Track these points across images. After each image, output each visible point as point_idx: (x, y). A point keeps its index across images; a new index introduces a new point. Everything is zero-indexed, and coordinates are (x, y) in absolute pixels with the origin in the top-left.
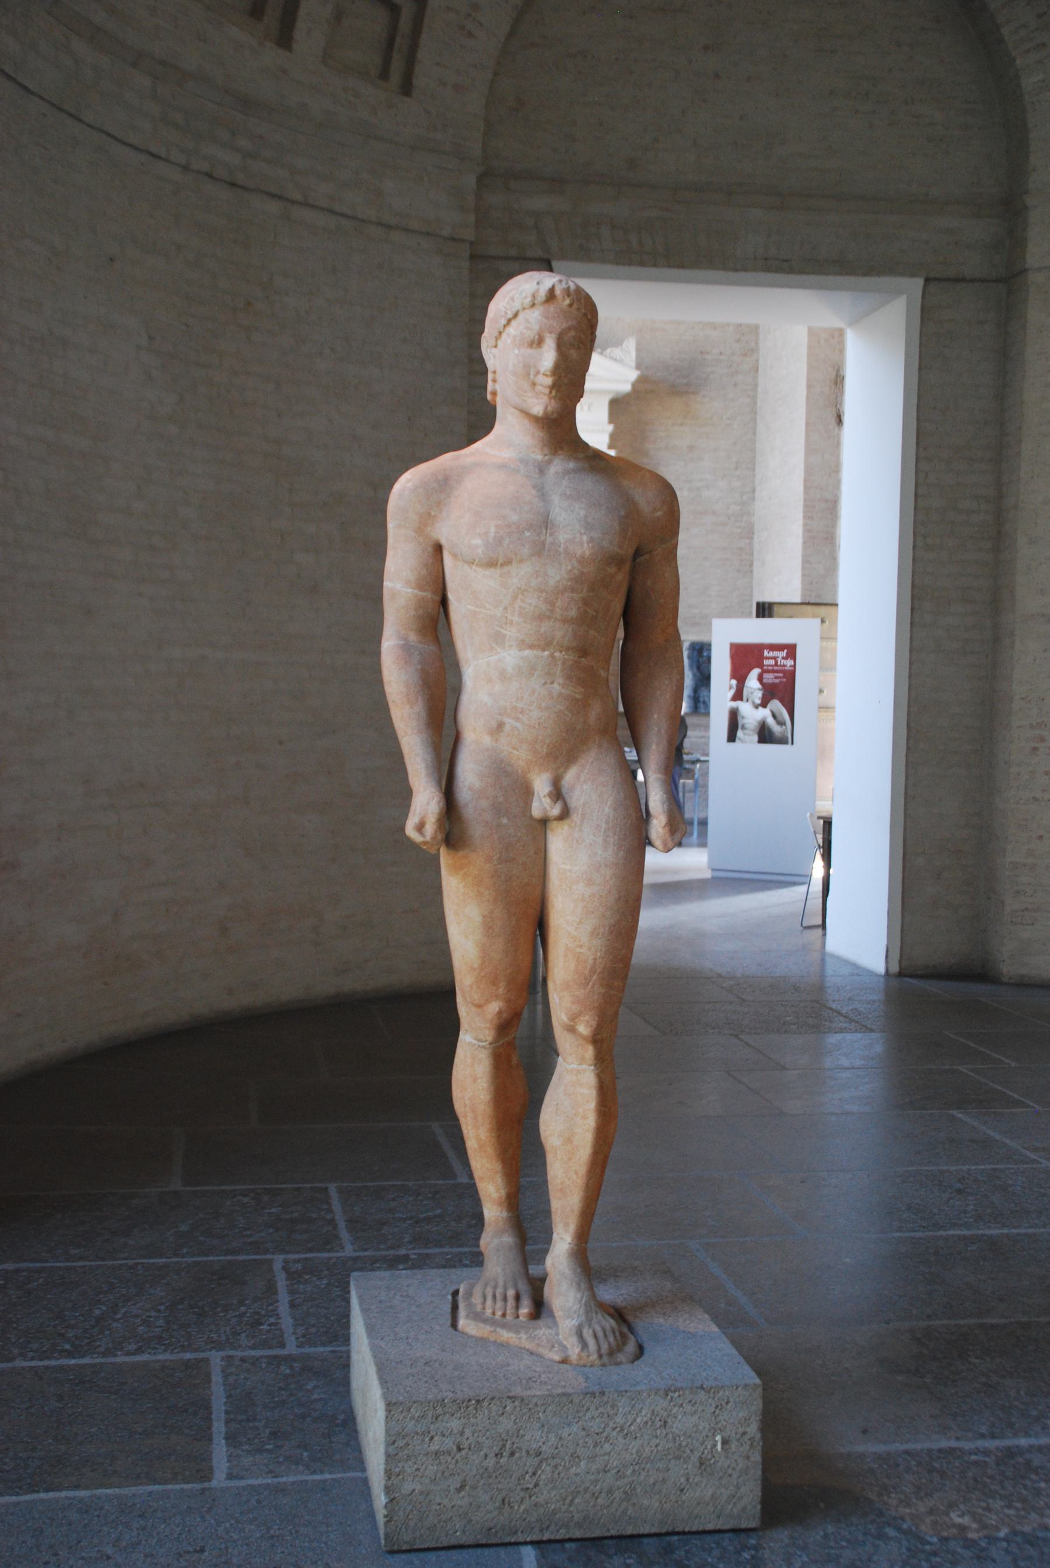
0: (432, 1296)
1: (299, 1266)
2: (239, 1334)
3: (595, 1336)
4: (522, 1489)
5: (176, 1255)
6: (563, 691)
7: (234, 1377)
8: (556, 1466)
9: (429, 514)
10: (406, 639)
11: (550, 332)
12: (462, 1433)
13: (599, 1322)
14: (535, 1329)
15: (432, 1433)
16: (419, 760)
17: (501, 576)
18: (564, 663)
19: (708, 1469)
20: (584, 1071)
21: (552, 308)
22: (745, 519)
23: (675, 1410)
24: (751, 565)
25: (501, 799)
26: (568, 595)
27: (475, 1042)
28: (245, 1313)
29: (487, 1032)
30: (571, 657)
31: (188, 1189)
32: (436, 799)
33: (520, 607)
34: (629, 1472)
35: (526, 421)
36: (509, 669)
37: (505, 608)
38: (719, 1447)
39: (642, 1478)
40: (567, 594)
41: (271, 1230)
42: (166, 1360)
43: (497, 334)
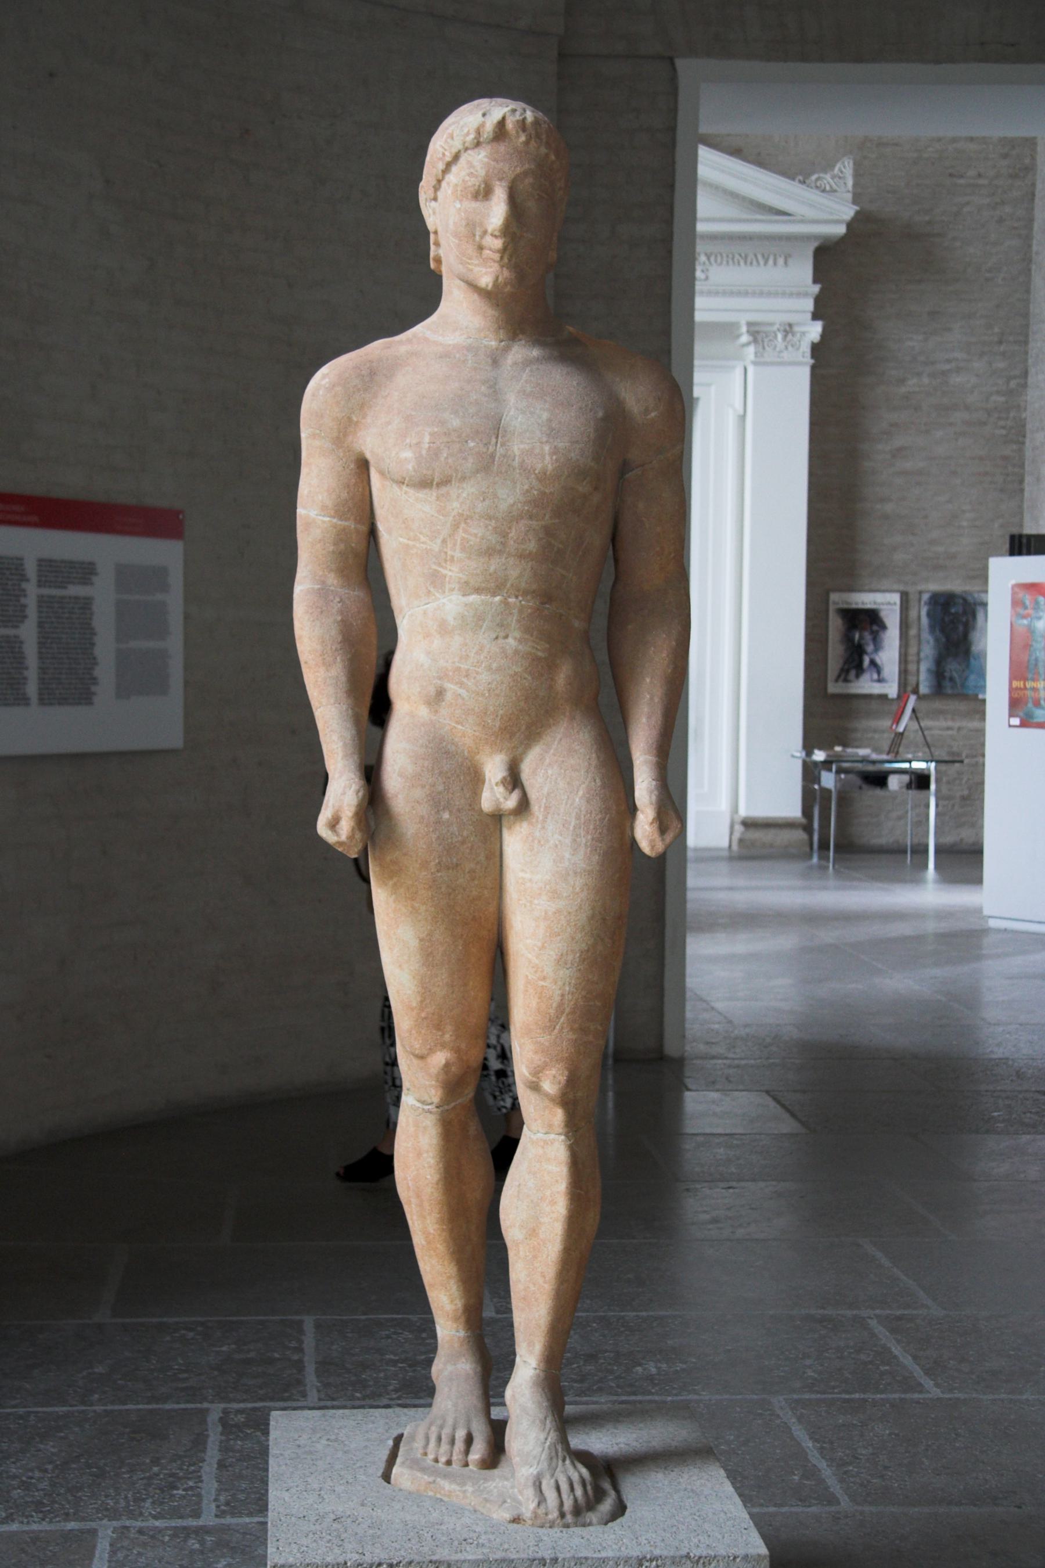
0: (368, 1440)
1: (241, 1418)
2: (144, 1500)
3: (558, 1489)
6: (520, 647)
7: (125, 1552)
9: (350, 419)
10: (323, 583)
11: (500, 180)
13: (565, 1471)
14: (486, 1480)
16: (335, 737)
17: (438, 499)
18: (521, 612)
20: (552, 1142)
21: (502, 148)
22: (1012, 415)
24: (1021, 481)
25: (441, 788)
27: (418, 1105)
28: (158, 1475)
29: (433, 1092)
30: (530, 603)
31: (119, 1320)
32: (355, 787)
33: (463, 539)
35: (476, 296)
37: (444, 541)
40: (523, 522)
41: (216, 1373)
42: (41, 1531)
43: (434, 182)
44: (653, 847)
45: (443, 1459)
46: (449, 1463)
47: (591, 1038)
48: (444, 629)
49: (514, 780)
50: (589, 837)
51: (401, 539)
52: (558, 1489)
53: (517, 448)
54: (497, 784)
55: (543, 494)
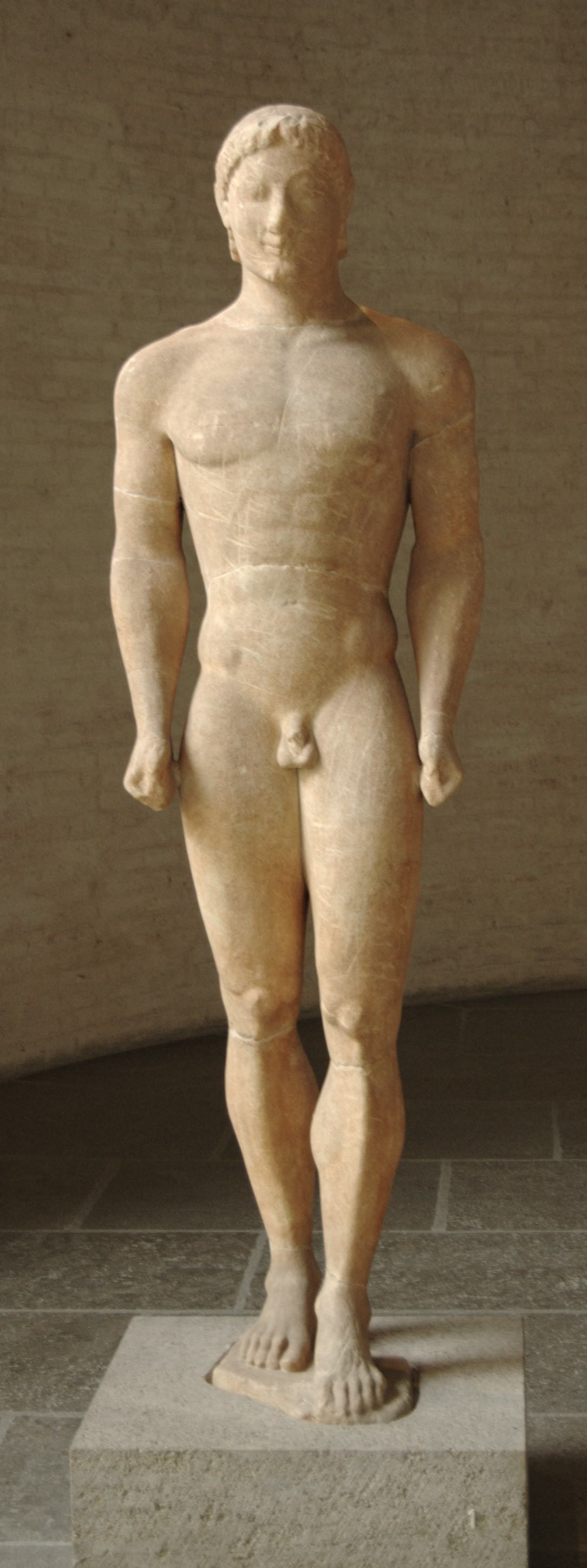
3: (347, 1391)
4: (234, 1559)
5: (28, 1306)
8: (273, 1534)
9: (153, 404)
11: (276, 182)
12: (160, 1489)
15: (126, 1487)
17: (227, 476)
19: (460, 1550)
21: (278, 152)
23: (416, 1477)
26: (306, 497)
27: (240, 1037)
30: (316, 570)
32: (155, 746)
34: (362, 1547)
36: (243, 587)
37: (235, 515)
38: (472, 1523)
39: (378, 1554)
44: (433, 797)
45: (258, 1362)
46: (263, 1365)
47: (383, 976)
48: (238, 596)
49: (306, 735)
50: (375, 789)
51: (201, 514)
52: (347, 1391)
53: (299, 426)
54: (290, 740)
55: (324, 469)
